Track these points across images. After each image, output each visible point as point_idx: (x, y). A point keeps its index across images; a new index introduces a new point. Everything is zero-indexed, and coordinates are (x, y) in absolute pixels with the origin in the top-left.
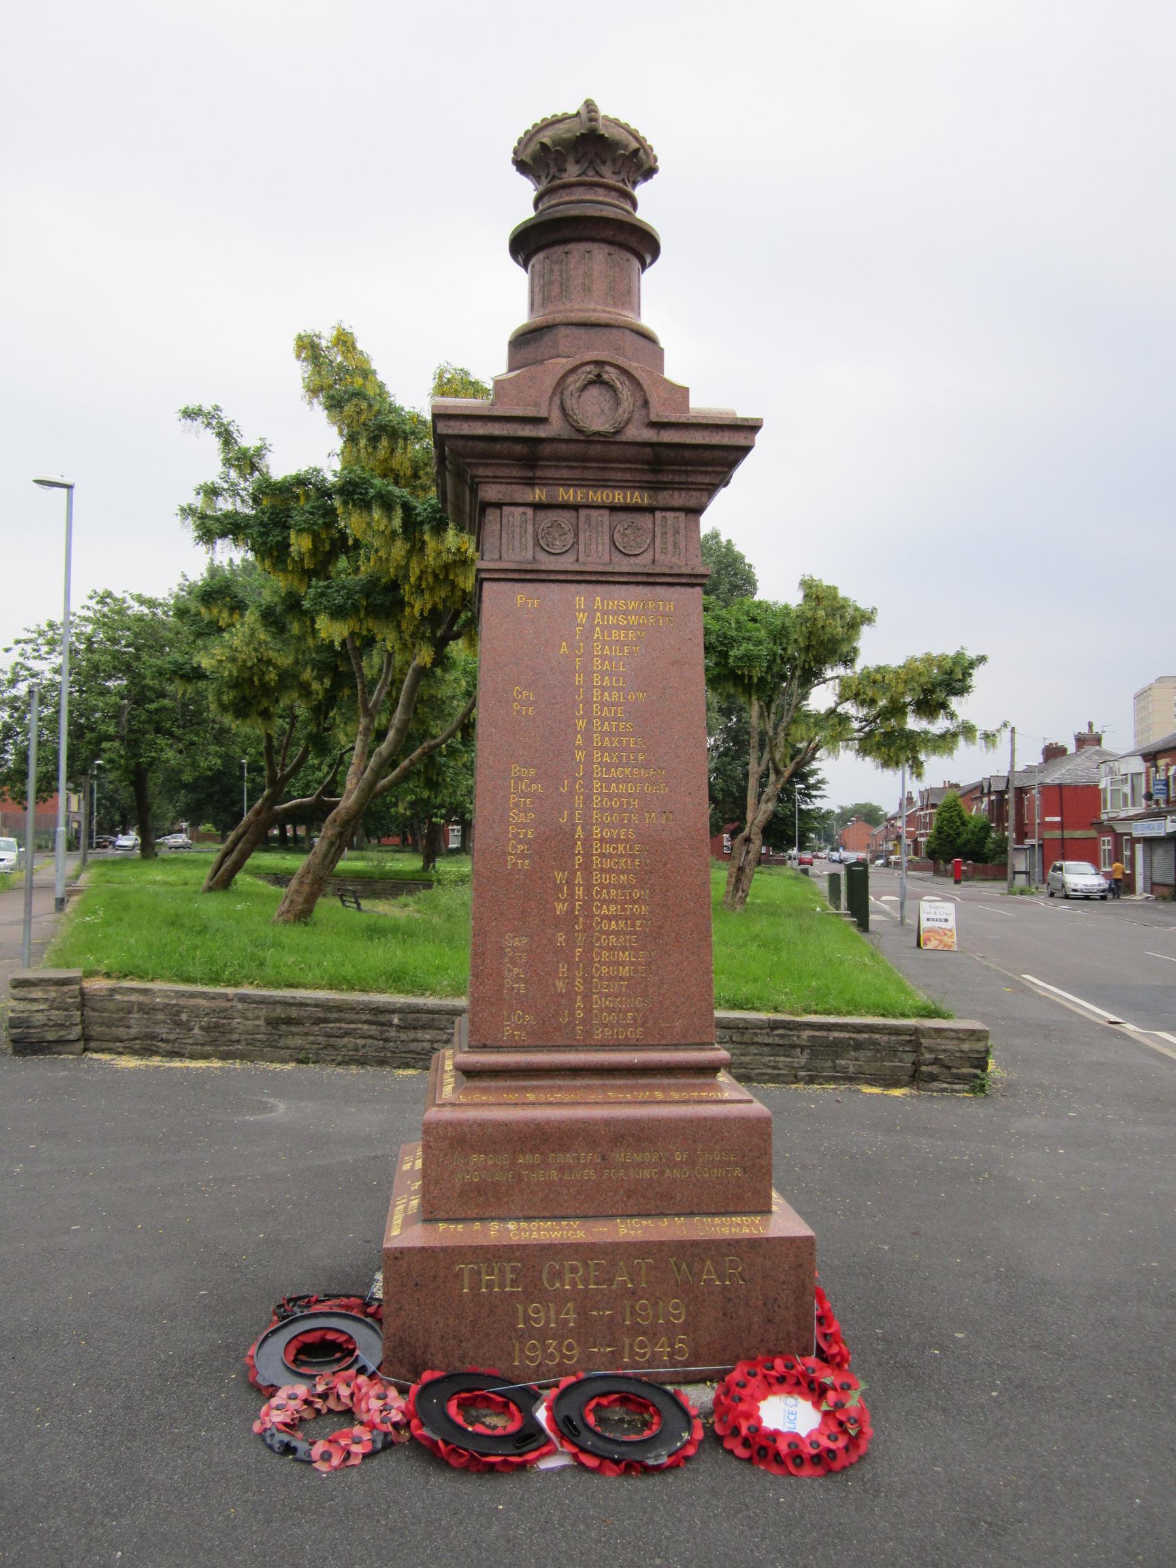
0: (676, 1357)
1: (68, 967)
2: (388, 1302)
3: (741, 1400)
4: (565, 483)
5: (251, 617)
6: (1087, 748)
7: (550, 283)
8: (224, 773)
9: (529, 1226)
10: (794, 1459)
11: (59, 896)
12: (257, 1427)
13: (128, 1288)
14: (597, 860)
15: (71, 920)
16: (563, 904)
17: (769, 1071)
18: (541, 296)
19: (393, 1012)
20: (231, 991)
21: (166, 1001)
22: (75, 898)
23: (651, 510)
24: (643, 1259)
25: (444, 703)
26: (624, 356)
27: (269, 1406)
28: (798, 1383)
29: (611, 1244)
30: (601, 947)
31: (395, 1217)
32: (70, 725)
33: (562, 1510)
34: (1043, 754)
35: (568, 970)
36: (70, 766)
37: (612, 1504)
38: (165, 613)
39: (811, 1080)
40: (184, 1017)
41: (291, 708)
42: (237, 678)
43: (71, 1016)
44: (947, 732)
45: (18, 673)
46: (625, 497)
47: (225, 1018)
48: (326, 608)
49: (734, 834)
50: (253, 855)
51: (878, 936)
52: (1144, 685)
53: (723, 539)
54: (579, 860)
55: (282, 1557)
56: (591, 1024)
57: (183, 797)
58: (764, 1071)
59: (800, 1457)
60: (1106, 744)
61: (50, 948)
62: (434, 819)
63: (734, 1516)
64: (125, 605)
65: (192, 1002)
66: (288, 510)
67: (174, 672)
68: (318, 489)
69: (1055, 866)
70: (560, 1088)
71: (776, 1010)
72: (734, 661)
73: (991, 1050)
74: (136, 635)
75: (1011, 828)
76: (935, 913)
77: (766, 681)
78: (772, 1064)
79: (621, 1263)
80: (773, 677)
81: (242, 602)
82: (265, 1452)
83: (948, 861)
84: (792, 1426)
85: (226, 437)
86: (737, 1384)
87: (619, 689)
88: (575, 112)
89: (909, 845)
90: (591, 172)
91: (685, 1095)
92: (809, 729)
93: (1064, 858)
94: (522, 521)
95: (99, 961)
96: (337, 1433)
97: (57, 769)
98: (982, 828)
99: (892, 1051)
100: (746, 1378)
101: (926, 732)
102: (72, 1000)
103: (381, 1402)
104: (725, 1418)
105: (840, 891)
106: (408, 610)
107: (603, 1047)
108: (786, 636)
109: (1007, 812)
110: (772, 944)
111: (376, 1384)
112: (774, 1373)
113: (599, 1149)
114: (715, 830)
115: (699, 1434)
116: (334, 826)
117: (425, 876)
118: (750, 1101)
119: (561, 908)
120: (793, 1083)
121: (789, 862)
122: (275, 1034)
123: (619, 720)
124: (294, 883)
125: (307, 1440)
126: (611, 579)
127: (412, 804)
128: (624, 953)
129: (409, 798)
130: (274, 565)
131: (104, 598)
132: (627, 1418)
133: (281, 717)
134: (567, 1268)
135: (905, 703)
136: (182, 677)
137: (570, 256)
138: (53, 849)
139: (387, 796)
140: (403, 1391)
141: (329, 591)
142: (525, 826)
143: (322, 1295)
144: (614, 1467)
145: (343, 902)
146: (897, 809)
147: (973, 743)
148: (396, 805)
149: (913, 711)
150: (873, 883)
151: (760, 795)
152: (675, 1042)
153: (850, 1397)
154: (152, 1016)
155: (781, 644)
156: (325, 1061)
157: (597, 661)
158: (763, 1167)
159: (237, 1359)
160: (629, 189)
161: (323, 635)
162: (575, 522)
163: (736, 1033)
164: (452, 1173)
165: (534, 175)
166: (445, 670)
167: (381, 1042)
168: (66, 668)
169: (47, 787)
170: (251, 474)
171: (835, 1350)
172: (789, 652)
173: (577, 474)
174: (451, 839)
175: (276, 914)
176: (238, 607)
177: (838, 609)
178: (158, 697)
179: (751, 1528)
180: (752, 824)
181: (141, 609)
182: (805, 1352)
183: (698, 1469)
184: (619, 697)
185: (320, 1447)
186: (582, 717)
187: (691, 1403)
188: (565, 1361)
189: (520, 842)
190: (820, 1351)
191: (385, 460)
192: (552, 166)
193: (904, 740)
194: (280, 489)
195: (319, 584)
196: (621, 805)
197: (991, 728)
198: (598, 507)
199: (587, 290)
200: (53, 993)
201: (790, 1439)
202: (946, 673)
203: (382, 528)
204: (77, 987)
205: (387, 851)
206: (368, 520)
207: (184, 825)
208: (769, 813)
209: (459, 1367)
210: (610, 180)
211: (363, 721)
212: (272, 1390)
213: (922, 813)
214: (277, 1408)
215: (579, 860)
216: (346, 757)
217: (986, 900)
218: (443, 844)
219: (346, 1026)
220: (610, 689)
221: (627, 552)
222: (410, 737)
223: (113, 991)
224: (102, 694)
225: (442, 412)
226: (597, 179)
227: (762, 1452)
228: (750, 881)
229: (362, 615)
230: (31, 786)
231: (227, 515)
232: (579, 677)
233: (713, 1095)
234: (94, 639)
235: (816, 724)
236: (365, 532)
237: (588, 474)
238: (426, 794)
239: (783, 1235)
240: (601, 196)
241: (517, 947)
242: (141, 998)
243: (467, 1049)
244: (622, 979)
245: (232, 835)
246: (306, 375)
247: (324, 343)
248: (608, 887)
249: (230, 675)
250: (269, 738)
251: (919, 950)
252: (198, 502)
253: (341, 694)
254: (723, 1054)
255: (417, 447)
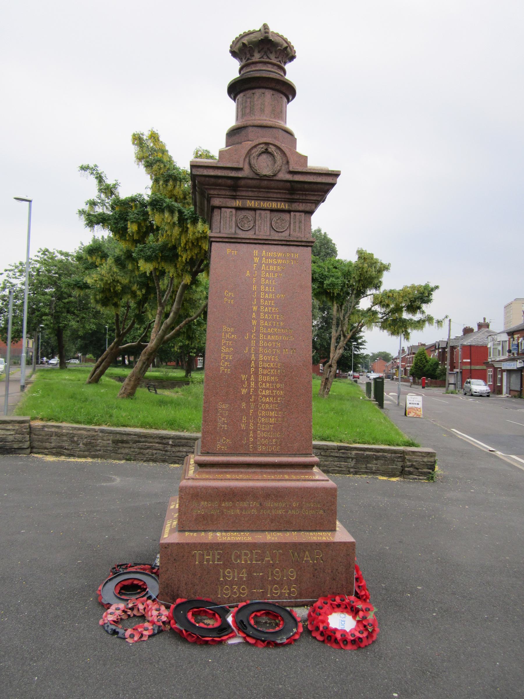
0: (291, 595)
1: (24, 415)
2: (162, 567)
3: (320, 614)
4: (250, 198)
5: (110, 261)
6: (483, 329)
7: (246, 107)
8: (98, 332)
9: (226, 535)
10: (343, 642)
11: (22, 384)
12: (101, 622)
13: (45, 558)
14: (261, 370)
15: (27, 395)
16: (245, 389)
17: (337, 469)
18: (241, 113)
19: (170, 438)
20: (97, 428)
21: (68, 431)
22: (29, 386)
23: (289, 211)
24: (278, 550)
25: (196, 301)
26: (278, 141)
27: (107, 613)
28: (346, 608)
29: (263, 543)
30: (262, 409)
31: (166, 529)
32: (28, 308)
33: (238, 662)
34: (463, 331)
35: (247, 419)
36: (28, 327)
37: (260, 660)
38: (72, 259)
39: (356, 473)
40: (76, 439)
41: (128, 303)
42: (103, 288)
43: (25, 437)
44: (420, 320)
45: (6, 284)
46: (277, 205)
47: (94, 440)
48: (143, 257)
49: (324, 364)
50: (109, 368)
51: (387, 411)
52: (509, 301)
53: (323, 232)
54: (253, 369)
55: (110, 681)
56: (256, 444)
57: (79, 342)
58: (335, 468)
59: (346, 640)
60: (491, 328)
61: (17, 407)
62: (191, 354)
63: (315, 667)
64: (54, 255)
65: (80, 432)
66: (127, 213)
67: (75, 285)
68: (141, 204)
69: (467, 381)
70: (242, 473)
71: (341, 441)
72: (326, 286)
73: (437, 461)
74: (59, 269)
75: (448, 364)
76: (413, 401)
77: (340, 295)
78: (339, 465)
79: (268, 552)
80: (343, 293)
81: (106, 254)
82: (106, 634)
83: (419, 378)
84: (343, 627)
85: (100, 179)
86: (319, 608)
87: (273, 293)
88: (259, 30)
89: (402, 371)
90: (265, 57)
91: (298, 477)
92: (359, 317)
93: (471, 378)
94: (230, 215)
95: (38, 413)
96: (137, 626)
97: (22, 328)
98: (435, 364)
99: (392, 461)
100: (322, 605)
101: (411, 320)
102: (26, 430)
103: (158, 612)
104: (313, 623)
105: (371, 390)
106: (180, 258)
107: (262, 454)
108: (350, 276)
109: (446, 357)
110: (340, 412)
111: (155, 604)
112: (335, 603)
113: (259, 501)
114: (315, 362)
115: (301, 630)
116: (145, 355)
117: (186, 379)
118: (328, 480)
119: (244, 391)
120: (348, 474)
121: (349, 377)
122: (116, 447)
123: (272, 307)
124: (127, 381)
125: (124, 629)
126: (270, 243)
127: (181, 347)
128: (272, 412)
129: (180, 344)
130: (120, 237)
131: (45, 252)
132: (269, 622)
133: (123, 307)
134: (243, 554)
135: (402, 306)
136: (79, 287)
137: (255, 95)
138: (20, 364)
139: (170, 343)
140: (168, 607)
141: (145, 249)
142: (229, 354)
143: (133, 563)
144: (262, 643)
145: (149, 390)
146: (397, 355)
147: (432, 325)
148: (174, 347)
149: (406, 310)
150: (386, 387)
151: (336, 347)
152: (294, 453)
153: (369, 614)
154: (61, 438)
155: (347, 279)
156: (138, 460)
157: (261, 370)
158: (333, 510)
159: (93, 591)
160: (283, 65)
161: (141, 269)
162: (254, 216)
163: (322, 450)
164: (192, 510)
165: (239, 58)
166: (197, 286)
167: (164, 452)
168: (27, 283)
169: (18, 336)
170: (111, 196)
171: (363, 593)
172: (351, 282)
173: (256, 194)
174: (198, 363)
175: (118, 394)
176: (104, 256)
177: (373, 263)
178: (68, 297)
179: (323, 672)
180: (333, 359)
181: (61, 257)
182: (350, 594)
183: (300, 645)
184: (272, 296)
185: (129, 632)
186: (256, 305)
187: (297, 615)
188: (241, 595)
189: (226, 361)
190: (356, 593)
191: (171, 191)
192: (248, 53)
193: (401, 323)
194: (124, 203)
195: (140, 246)
196: (273, 345)
197: (440, 318)
198: (265, 210)
199: (262, 111)
200: (17, 427)
201: (342, 633)
202: (421, 293)
203: (169, 221)
204: (28, 424)
205: (169, 368)
206: (163, 217)
207: (80, 355)
208: (340, 354)
209: (193, 597)
210: (274, 61)
211: (159, 308)
212: (109, 605)
213: (408, 357)
214: (111, 614)
215: (253, 369)
216: (152, 325)
217: (435, 396)
218: (195, 366)
219: (148, 444)
220: (269, 293)
221: (278, 230)
222: (180, 316)
223: (44, 426)
224: (43, 295)
225: (195, 164)
226: (268, 60)
227: (329, 638)
228: (331, 384)
229: (159, 260)
230: (10, 335)
231: (99, 215)
232: (255, 287)
233: (311, 477)
234: (40, 270)
235: (362, 315)
236: (161, 223)
237: (260, 195)
238: (187, 342)
239: (341, 541)
240: (269, 68)
241: (223, 409)
242: (56, 430)
243: (200, 454)
244: (271, 424)
245: (100, 360)
246: (137, 152)
247: (145, 138)
248: (265, 382)
249: (100, 287)
250: (117, 315)
251: (406, 417)
252: (87, 208)
253: (150, 297)
254: (316, 459)
255: (186, 186)
